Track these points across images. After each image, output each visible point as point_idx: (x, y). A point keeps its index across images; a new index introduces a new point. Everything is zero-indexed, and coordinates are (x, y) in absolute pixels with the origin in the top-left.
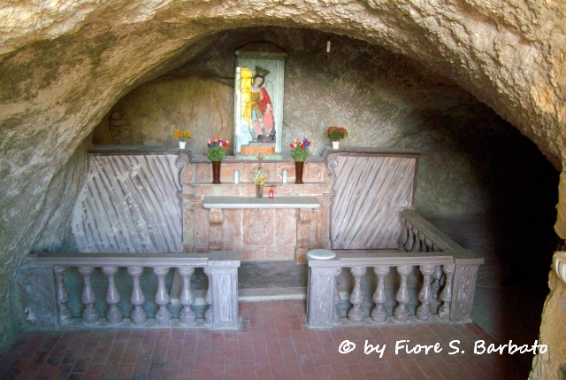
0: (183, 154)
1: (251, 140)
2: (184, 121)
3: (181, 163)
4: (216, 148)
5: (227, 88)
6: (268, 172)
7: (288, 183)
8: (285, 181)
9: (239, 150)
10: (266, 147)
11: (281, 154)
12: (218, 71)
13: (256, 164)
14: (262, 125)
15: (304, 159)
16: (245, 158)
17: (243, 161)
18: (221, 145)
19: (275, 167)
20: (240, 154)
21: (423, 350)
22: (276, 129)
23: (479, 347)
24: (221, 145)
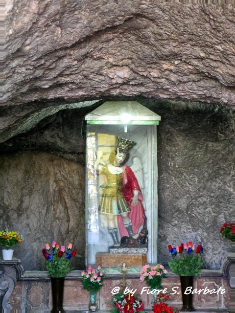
1: (112, 244)
2: (8, 218)
5: (75, 167)
9: (92, 260)
10: (136, 252)
12: (60, 143)
23: (188, 290)
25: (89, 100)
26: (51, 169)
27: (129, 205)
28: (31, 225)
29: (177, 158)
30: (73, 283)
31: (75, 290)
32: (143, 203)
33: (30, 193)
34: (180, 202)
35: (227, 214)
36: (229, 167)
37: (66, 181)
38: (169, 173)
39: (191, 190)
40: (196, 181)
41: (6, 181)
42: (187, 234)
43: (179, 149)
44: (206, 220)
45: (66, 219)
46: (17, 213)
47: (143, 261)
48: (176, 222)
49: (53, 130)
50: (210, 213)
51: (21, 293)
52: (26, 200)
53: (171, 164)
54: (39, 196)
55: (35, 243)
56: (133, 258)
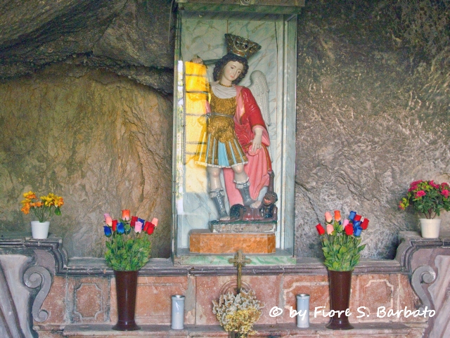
0: (38, 252)
1: (214, 216)
2: (54, 177)
3: (35, 277)
4: (128, 238)
5: (154, 100)
6: (259, 297)
7: (313, 326)
8: (303, 322)
9: (183, 242)
10: (252, 233)
11: (287, 252)
12: (131, 51)
13: (227, 279)
14: (242, 180)
15: (352, 265)
16: (199, 263)
17: (194, 271)
18: (138, 228)
19: (277, 284)
20: (191, 251)
21: (336, 314)
22: (277, 188)
24: (138, 228)
25: (174, 48)
26: (118, 105)
27: (245, 152)
28: (88, 187)
29: (322, 78)
30: (150, 281)
31: (155, 292)
32: (269, 149)
33: (87, 141)
34: (323, 151)
35: (398, 170)
36: (407, 95)
37: (140, 124)
38: (308, 104)
39: (343, 131)
40: (351, 117)
41: (51, 120)
42: (328, 203)
43: (326, 63)
44: (363, 180)
45: (140, 180)
46: (68, 169)
47: (269, 245)
48: (314, 184)
49: (120, 26)
50: (369, 169)
51: (63, 294)
52: (81, 151)
53: (312, 88)
54: (99, 145)
55: (94, 214)
56: (253, 240)
